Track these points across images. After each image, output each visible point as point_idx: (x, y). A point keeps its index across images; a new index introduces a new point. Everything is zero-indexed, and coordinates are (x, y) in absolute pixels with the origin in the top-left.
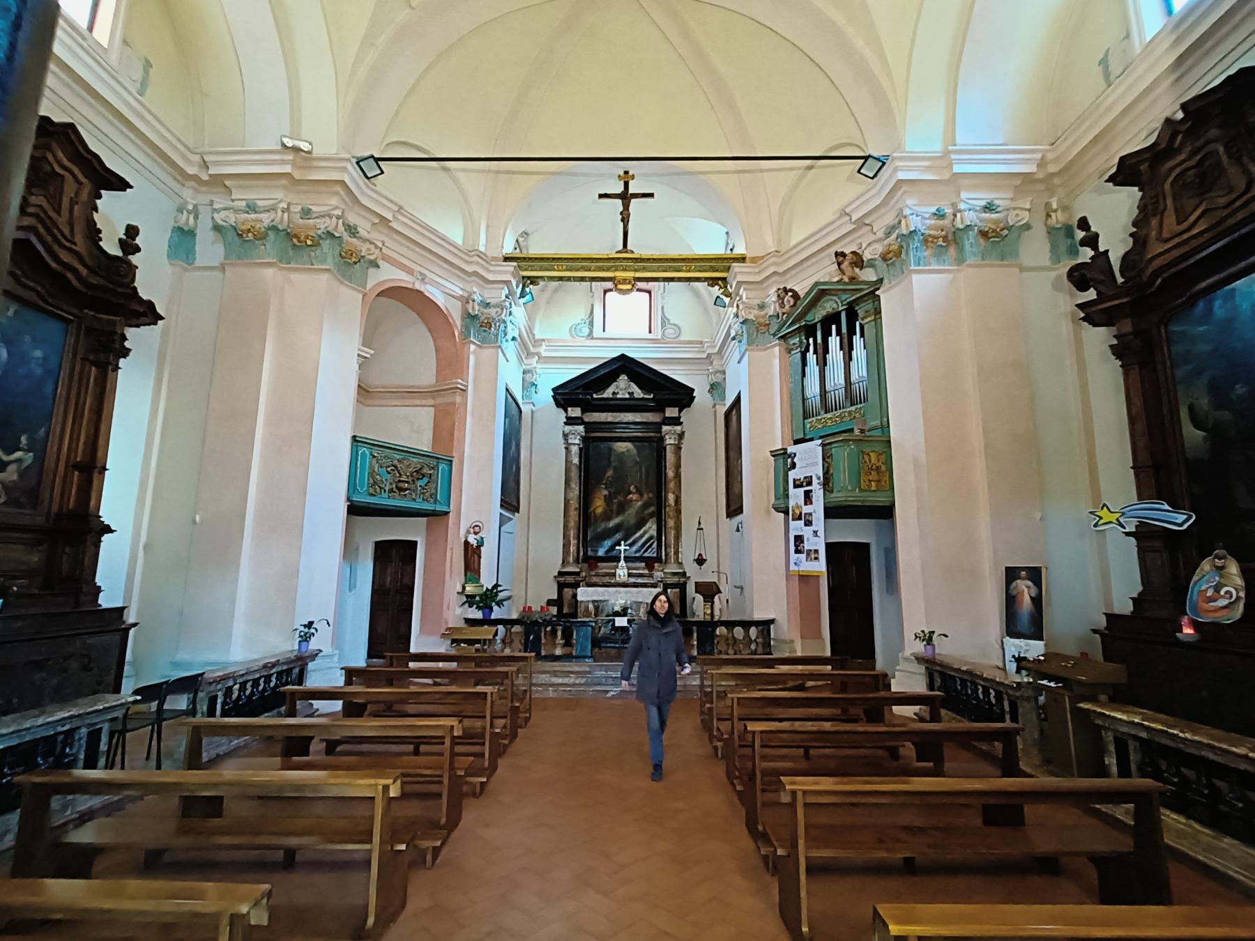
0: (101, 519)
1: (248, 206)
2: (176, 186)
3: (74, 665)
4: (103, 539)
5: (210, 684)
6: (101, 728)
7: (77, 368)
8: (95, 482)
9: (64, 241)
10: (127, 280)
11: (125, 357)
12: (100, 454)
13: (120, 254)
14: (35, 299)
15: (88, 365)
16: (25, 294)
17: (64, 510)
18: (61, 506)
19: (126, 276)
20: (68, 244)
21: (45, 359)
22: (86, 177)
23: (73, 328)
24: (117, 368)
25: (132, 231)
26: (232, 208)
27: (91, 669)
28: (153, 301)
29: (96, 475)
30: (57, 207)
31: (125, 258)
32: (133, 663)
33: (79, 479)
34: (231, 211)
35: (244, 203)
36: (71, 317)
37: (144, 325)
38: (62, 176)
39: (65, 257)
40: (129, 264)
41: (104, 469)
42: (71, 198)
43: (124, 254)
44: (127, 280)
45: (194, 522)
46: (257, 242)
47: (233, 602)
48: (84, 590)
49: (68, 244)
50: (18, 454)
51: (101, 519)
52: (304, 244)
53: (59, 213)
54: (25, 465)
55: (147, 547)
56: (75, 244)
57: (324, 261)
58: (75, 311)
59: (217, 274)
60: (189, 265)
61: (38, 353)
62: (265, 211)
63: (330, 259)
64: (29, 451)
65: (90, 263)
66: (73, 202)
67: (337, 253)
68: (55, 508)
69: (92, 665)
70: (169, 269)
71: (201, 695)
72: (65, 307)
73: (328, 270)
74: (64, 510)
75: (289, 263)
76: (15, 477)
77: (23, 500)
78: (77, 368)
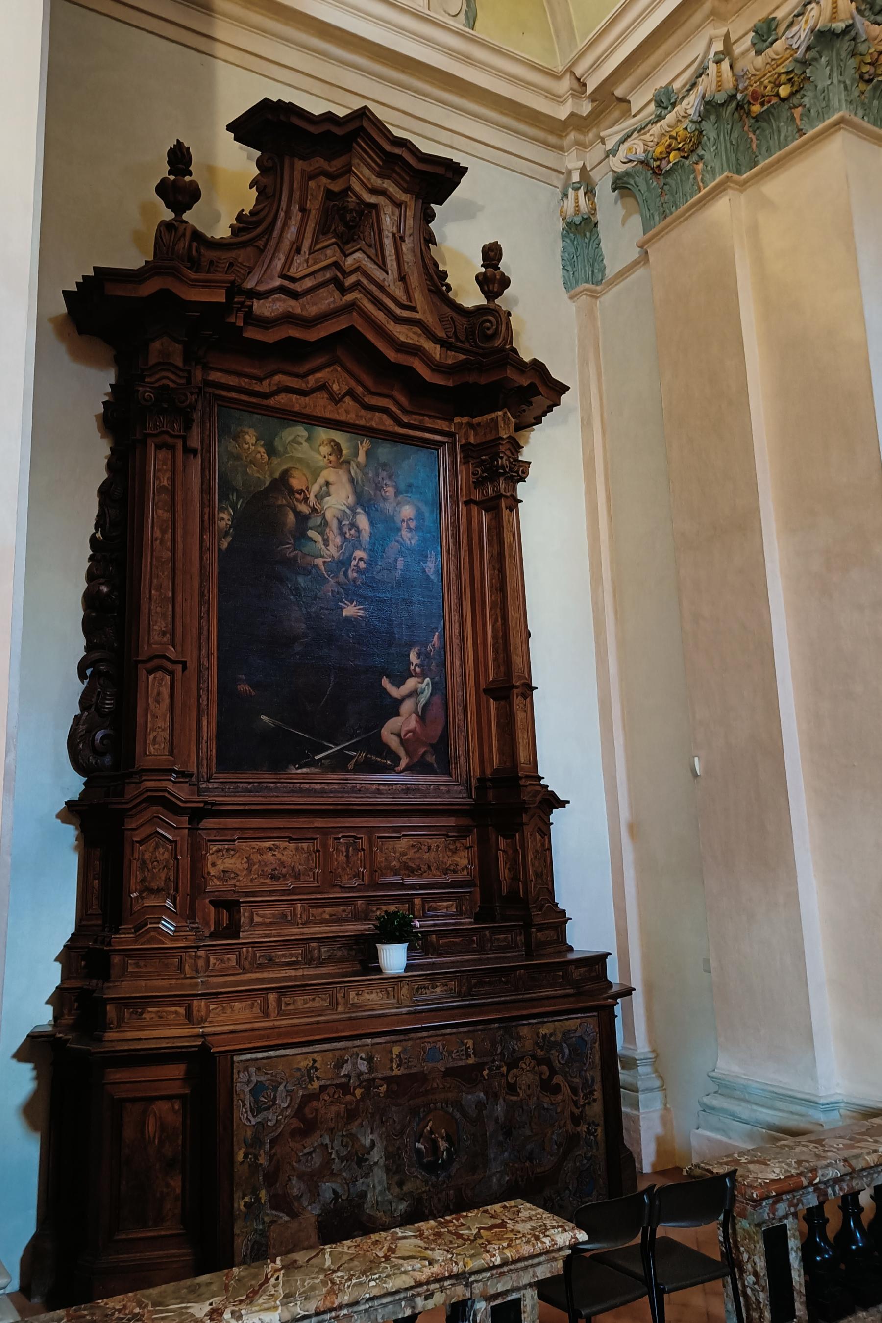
0: (542, 782)
1: (659, 104)
2: (548, 157)
3: (526, 1078)
4: (552, 818)
5: (757, 1203)
6: (518, 1301)
7: (463, 520)
8: (520, 716)
9: (398, 311)
10: (498, 343)
11: (523, 479)
12: (517, 660)
13: (484, 302)
14: (388, 424)
15: (475, 509)
16: (379, 421)
17: (488, 772)
18: (483, 771)
19: (496, 334)
20: (406, 314)
21: (420, 515)
22: (405, 191)
23: (444, 453)
24: (516, 502)
25: (492, 254)
26: (635, 130)
27: (557, 1089)
28: (277, 94)
29: (518, 701)
30: (380, 263)
31: (491, 306)
32: (656, 1060)
33: (497, 709)
34: (635, 134)
35: (652, 106)
36: (438, 438)
37: (544, 414)
38: (375, 206)
39: (403, 334)
40: (495, 312)
41: (529, 688)
42: (394, 235)
43: (488, 301)
44: (498, 343)
45: (695, 775)
46: (687, 162)
47: (800, 954)
48: (537, 920)
49: (406, 314)
50: (411, 683)
51: (542, 782)
52: (775, 100)
53: (384, 268)
54: (423, 700)
55: (634, 829)
56: (413, 309)
57: (827, 109)
58: (443, 425)
59: (640, 272)
60: (598, 283)
61: (407, 511)
62: (689, 91)
63: (838, 96)
64: (423, 675)
65: (441, 334)
66: (398, 240)
67: (850, 71)
68: (476, 772)
69: (558, 1079)
70: (572, 307)
71: (743, 1224)
72: (429, 423)
73: (842, 121)
74: (488, 772)
75: (756, 164)
76: (413, 723)
77: (431, 759)
78: (463, 520)
